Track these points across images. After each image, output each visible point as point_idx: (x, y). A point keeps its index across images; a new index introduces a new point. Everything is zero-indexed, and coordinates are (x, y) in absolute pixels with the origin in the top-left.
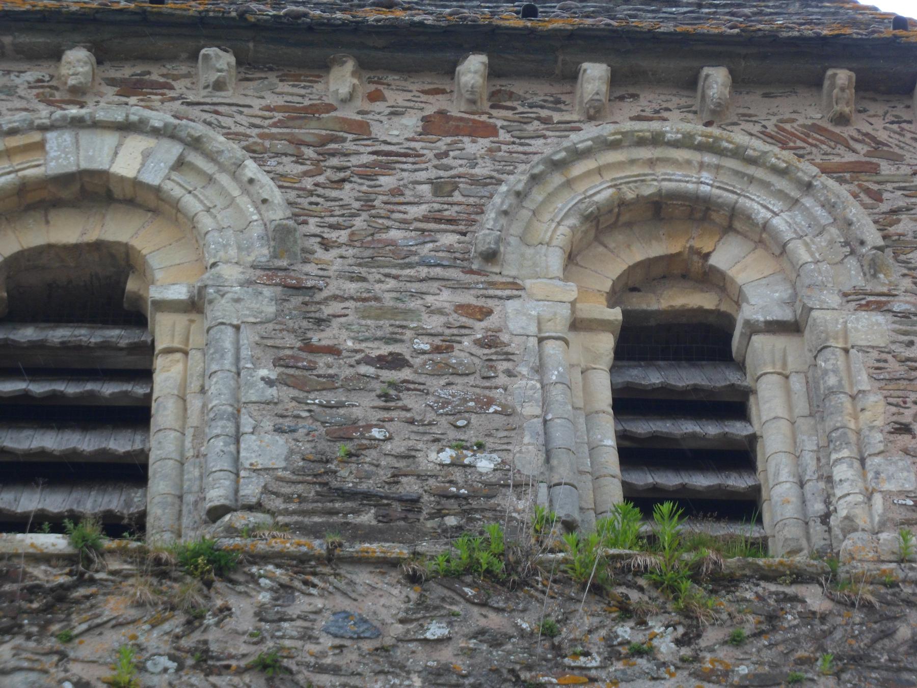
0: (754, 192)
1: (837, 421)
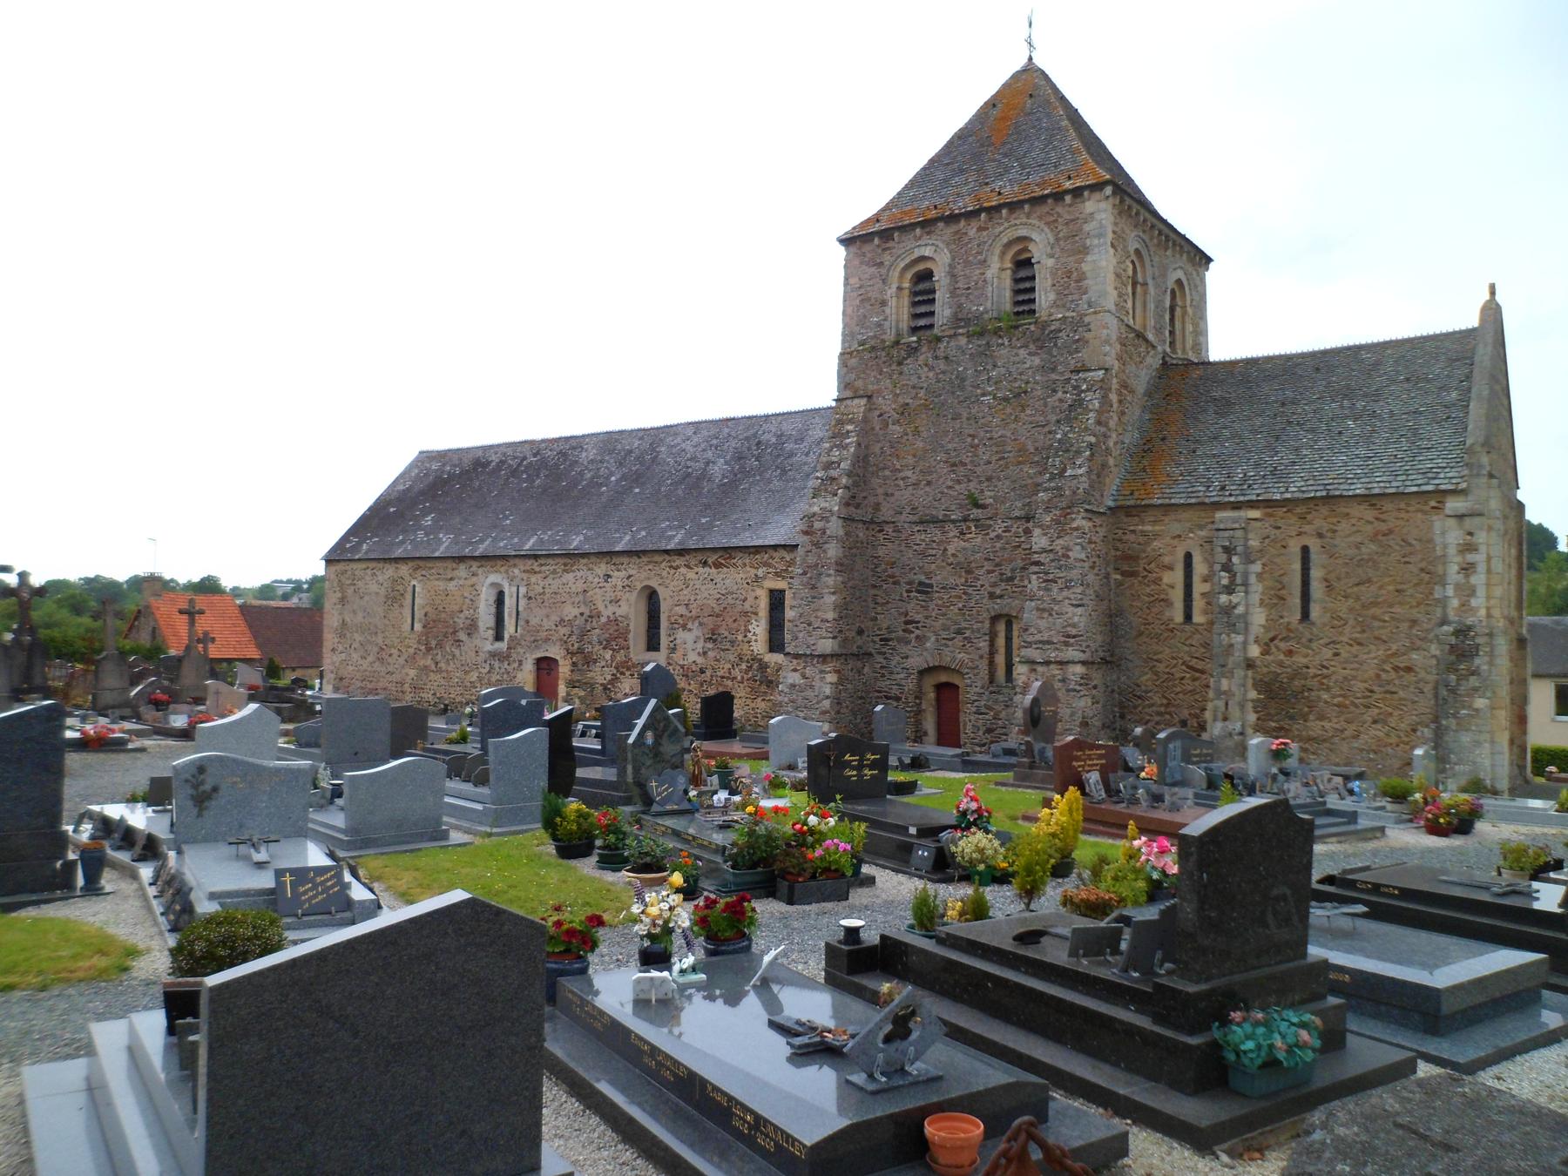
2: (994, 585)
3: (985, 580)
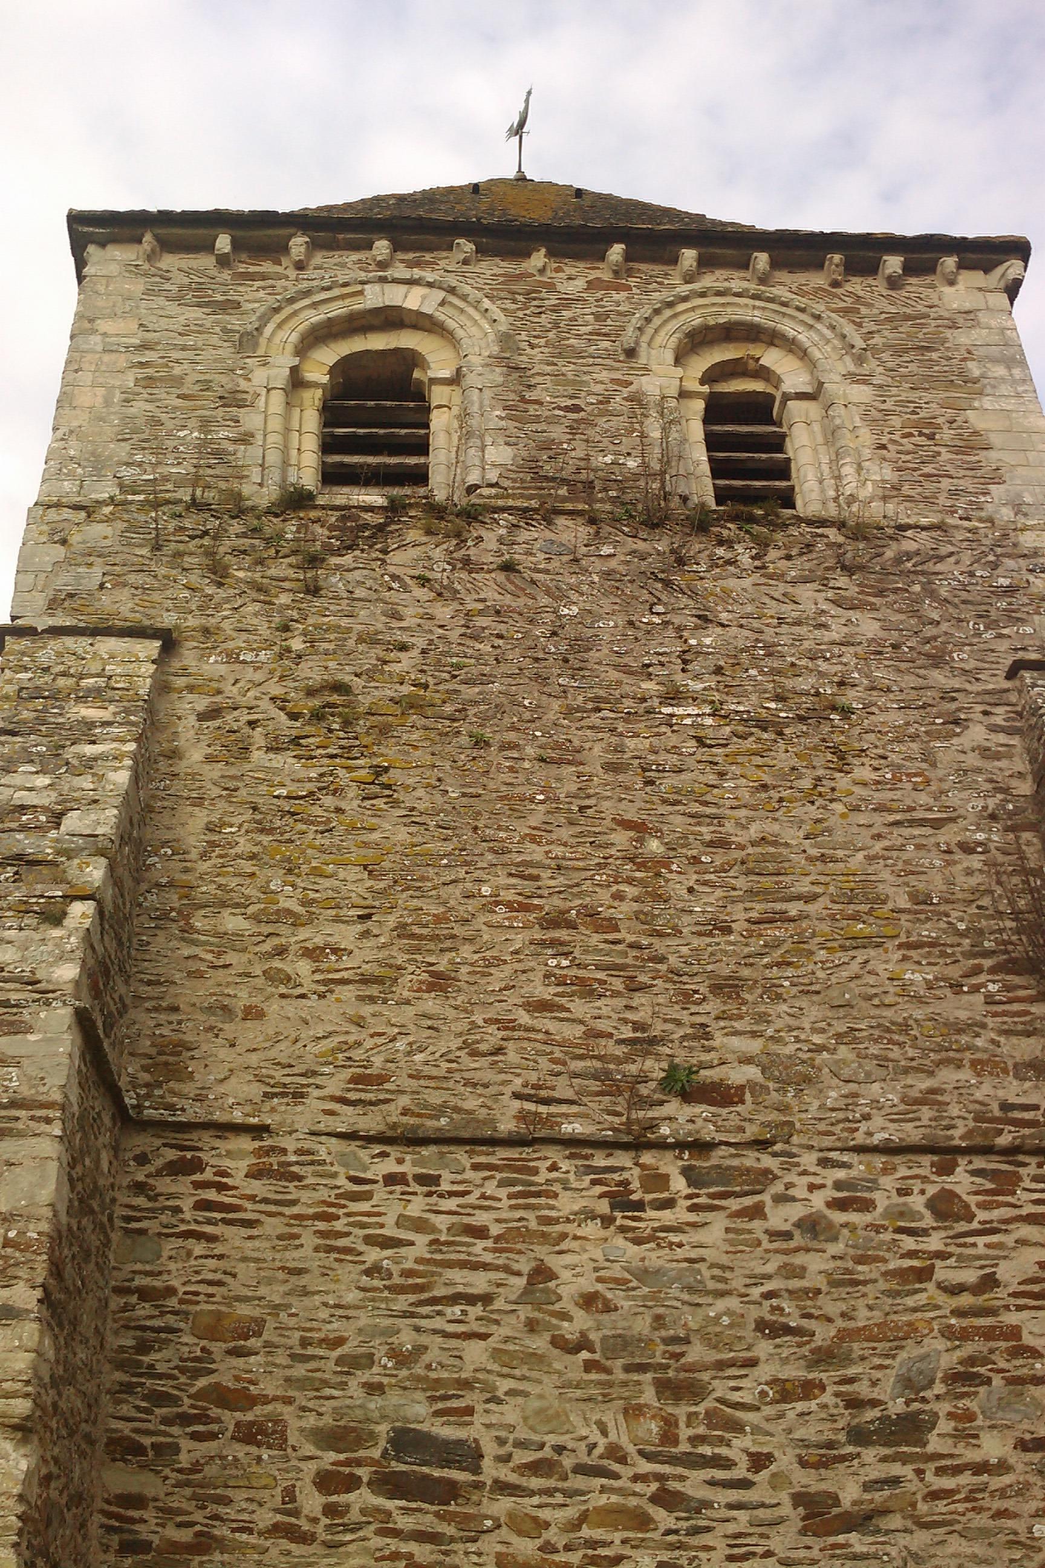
0: (786, 320)
1: (842, 443)
2: (823, 1457)
3: (785, 1434)
